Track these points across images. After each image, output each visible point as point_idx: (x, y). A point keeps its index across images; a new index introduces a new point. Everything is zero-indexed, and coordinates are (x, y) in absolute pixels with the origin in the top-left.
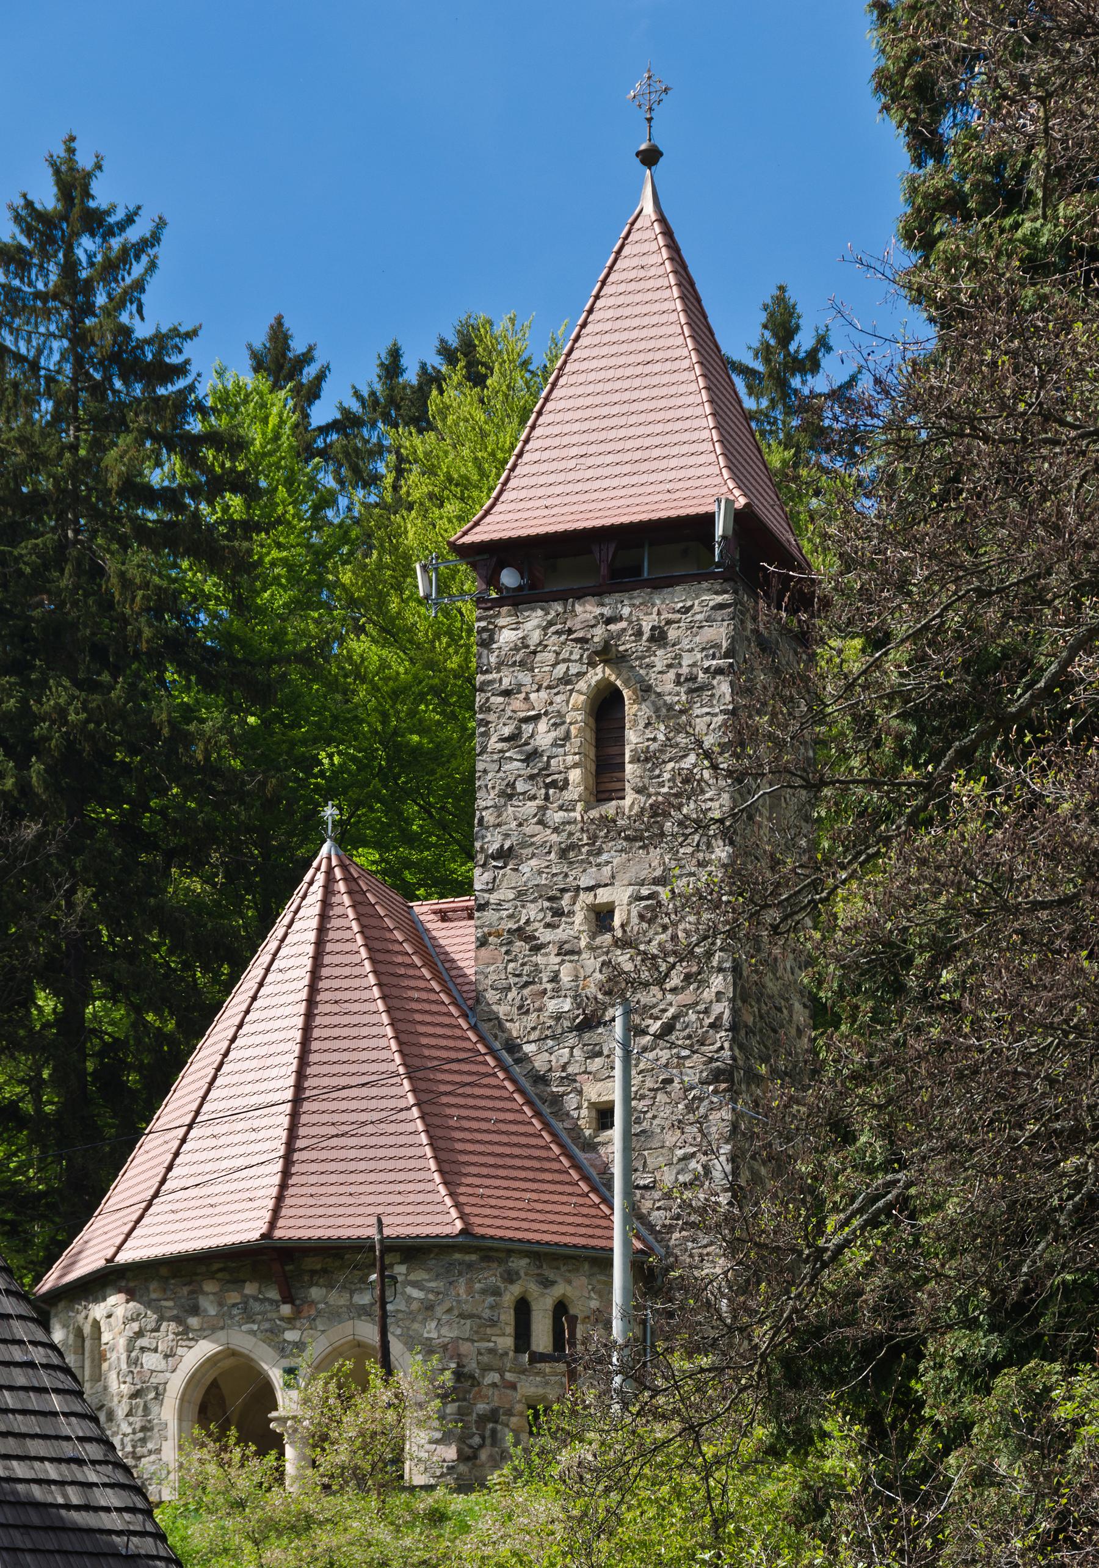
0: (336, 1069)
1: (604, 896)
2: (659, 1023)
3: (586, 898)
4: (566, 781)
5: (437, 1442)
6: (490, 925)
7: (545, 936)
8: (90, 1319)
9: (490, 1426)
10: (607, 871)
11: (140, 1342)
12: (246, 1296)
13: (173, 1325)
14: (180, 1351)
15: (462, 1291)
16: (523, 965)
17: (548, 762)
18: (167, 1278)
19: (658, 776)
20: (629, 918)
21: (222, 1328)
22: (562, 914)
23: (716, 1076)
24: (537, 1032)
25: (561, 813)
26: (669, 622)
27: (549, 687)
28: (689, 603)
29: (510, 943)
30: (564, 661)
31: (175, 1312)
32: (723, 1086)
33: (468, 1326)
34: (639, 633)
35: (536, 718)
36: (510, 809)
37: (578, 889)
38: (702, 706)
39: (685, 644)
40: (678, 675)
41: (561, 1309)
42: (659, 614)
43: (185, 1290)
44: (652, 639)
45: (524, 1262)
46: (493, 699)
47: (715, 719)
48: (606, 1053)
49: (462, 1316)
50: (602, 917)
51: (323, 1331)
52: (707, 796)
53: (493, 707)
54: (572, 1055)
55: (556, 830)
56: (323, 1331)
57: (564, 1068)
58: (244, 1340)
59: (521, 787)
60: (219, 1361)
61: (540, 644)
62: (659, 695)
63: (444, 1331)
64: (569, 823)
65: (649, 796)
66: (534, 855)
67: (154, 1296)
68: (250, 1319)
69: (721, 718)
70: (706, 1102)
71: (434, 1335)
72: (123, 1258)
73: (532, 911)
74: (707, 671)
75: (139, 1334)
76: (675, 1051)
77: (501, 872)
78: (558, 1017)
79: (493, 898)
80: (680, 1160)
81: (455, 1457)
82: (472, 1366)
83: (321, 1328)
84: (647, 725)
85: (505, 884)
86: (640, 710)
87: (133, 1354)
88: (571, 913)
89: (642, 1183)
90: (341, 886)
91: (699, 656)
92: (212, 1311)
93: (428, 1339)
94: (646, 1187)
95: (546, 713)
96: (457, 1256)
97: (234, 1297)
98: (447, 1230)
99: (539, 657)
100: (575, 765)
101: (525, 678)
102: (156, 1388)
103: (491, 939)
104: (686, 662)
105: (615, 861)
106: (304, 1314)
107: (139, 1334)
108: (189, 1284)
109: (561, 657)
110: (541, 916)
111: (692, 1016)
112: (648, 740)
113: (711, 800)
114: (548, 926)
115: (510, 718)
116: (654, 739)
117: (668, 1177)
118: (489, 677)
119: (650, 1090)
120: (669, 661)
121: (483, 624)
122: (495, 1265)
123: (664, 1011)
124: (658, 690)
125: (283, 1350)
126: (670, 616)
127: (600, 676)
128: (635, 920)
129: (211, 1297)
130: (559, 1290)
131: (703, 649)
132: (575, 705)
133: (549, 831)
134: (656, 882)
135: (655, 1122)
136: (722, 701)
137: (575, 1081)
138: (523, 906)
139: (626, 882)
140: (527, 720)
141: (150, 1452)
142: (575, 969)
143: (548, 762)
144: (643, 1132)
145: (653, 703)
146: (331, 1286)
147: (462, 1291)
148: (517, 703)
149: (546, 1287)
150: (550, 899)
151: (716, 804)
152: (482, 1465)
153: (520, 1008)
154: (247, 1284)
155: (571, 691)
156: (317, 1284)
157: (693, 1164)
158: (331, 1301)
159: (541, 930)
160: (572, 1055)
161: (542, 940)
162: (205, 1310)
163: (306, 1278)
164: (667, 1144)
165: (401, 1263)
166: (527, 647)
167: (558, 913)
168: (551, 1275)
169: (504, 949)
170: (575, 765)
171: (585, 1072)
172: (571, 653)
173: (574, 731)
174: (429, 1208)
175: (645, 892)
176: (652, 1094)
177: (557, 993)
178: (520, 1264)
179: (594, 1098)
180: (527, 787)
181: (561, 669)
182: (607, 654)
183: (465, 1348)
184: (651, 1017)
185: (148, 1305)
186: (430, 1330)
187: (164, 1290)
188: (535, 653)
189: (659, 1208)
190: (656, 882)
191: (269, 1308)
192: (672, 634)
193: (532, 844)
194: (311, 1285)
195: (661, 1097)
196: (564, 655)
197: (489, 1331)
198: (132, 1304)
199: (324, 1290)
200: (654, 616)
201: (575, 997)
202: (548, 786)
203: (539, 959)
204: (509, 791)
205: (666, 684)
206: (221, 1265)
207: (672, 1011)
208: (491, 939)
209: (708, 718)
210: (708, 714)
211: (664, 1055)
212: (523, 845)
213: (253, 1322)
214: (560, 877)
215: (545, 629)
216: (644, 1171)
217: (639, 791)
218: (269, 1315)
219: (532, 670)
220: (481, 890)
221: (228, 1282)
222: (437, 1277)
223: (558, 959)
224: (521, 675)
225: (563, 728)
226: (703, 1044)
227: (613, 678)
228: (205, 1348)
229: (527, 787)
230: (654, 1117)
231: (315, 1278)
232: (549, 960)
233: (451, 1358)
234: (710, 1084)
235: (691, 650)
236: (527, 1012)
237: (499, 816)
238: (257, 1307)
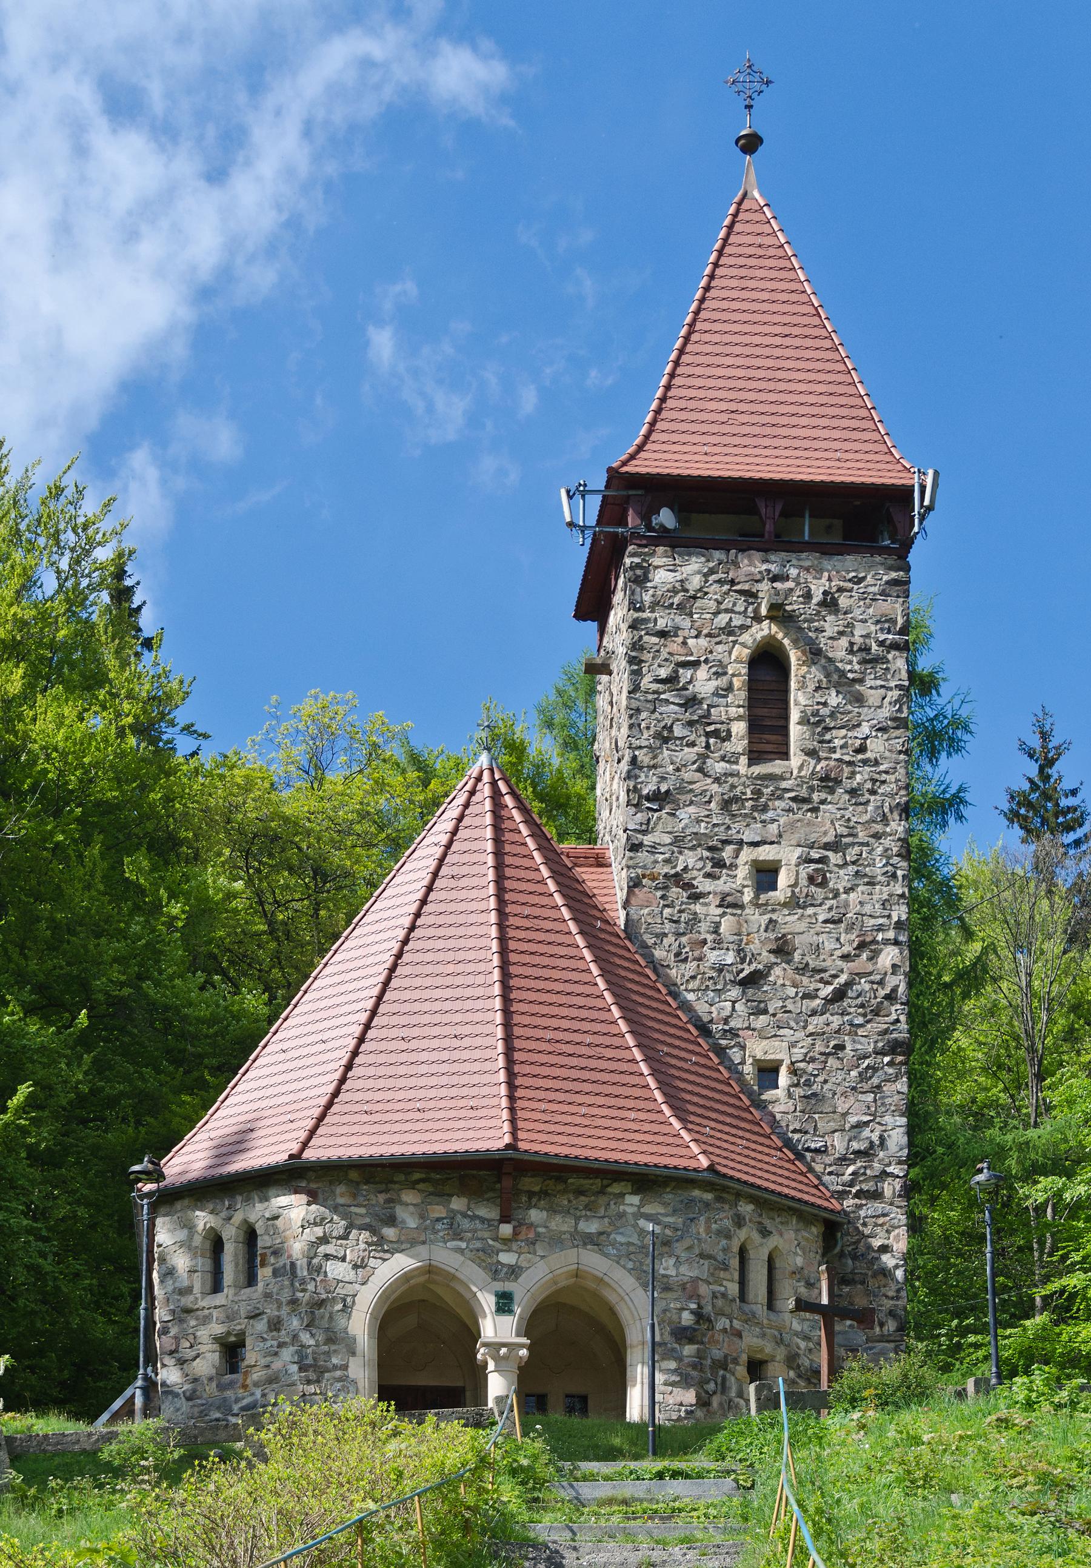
0: (541, 984)
1: (766, 853)
2: (830, 988)
3: (747, 855)
4: (729, 732)
5: (673, 1384)
6: (644, 867)
7: (704, 885)
9: (721, 1372)
10: (773, 828)
11: (323, 1249)
12: (453, 1211)
13: (365, 1235)
14: (372, 1262)
15: (701, 1230)
16: (680, 911)
17: (708, 710)
18: (358, 1183)
19: (829, 742)
20: (797, 879)
21: (424, 1243)
22: (724, 866)
23: (894, 1048)
24: (697, 982)
25: (723, 764)
26: (840, 590)
27: (709, 635)
28: (862, 575)
29: (666, 888)
30: (727, 611)
31: (367, 1220)
32: (900, 1058)
33: (706, 1267)
34: (808, 596)
35: (696, 664)
36: (666, 753)
37: (741, 843)
38: (875, 678)
39: (857, 613)
40: (852, 644)
42: (830, 580)
43: (381, 1198)
44: (823, 604)
45: (750, 1207)
46: (646, 638)
47: (890, 694)
48: (771, 1011)
49: (702, 1256)
50: (765, 875)
51: (543, 1257)
52: (882, 768)
53: (647, 646)
54: (733, 1009)
55: (717, 780)
56: (543, 1257)
57: (726, 1021)
58: (448, 1256)
59: (678, 731)
60: (412, 1278)
61: (700, 590)
62: (830, 660)
63: (683, 1269)
64: (732, 775)
65: (819, 760)
66: (692, 803)
68: (458, 1236)
69: (896, 693)
70: (880, 1073)
71: (672, 1272)
72: (309, 1155)
73: (689, 859)
74: (881, 644)
75: (324, 1240)
76: (846, 1018)
77: (656, 815)
78: (720, 969)
79: (647, 840)
80: (853, 1127)
81: (694, 1401)
82: (708, 1309)
83: (540, 1253)
84: (818, 689)
85: (660, 827)
86: (809, 672)
87: (315, 1261)
88: (733, 866)
89: (813, 1146)
90: (508, 800)
91: (873, 628)
92: (412, 1223)
93: (664, 1276)
94: (817, 1151)
95: (706, 661)
96: (696, 1193)
97: (438, 1211)
98: (693, 1164)
99: (699, 603)
100: (739, 718)
101: (685, 623)
102: (344, 1300)
103: (644, 881)
104: (858, 632)
105: (782, 820)
106: (522, 1237)
107: (324, 1240)
108: (387, 1191)
109: (723, 607)
110: (700, 864)
111: (864, 985)
112: (818, 703)
113: (887, 772)
114: (708, 875)
115: (666, 660)
116: (825, 704)
117: (839, 1143)
118: (645, 615)
119: (821, 1054)
120: (841, 629)
121: (637, 560)
122: (727, 1207)
123: (835, 976)
124: (830, 655)
125: (495, 1272)
126: (842, 584)
127: (766, 632)
128: (803, 882)
129: (411, 1208)
130: (774, 1241)
131: (878, 622)
132: (737, 657)
133: (709, 781)
134: (826, 846)
135: (826, 1087)
136: (897, 676)
137: (738, 1036)
138: (680, 853)
139: (794, 842)
140: (685, 665)
141: (336, 1367)
142: (738, 922)
143: (708, 710)
144: (814, 1095)
145: (824, 668)
146: (553, 1210)
147: (701, 1230)
148: (674, 646)
149: (764, 1236)
150: (710, 849)
151: (892, 778)
152: (715, 1413)
153: (677, 955)
154: (454, 1199)
155: (735, 642)
156: (535, 1206)
157: (866, 1133)
158: (553, 1225)
159: (700, 879)
160: (733, 1009)
161: (700, 889)
162: (403, 1222)
163: (524, 1199)
164: (839, 1110)
165: (633, 1193)
166: (687, 591)
167: (719, 864)
168: (767, 1223)
169: (659, 894)
170: (739, 718)
171: (748, 1028)
172: (734, 604)
173: (737, 683)
174: (660, 1139)
175: (815, 854)
176: (823, 1058)
177: (718, 944)
178: (746, 1209)
179: (759, 1055)
180: (685, 732)
181: (722, 619)
182: (779, 614)
183: (704, 1289)
184: (821, 980)
185: (335, 1209)
186: (667, 1267)
187: (354, 1196)
188: (694, 598)
189: (830, 1173)
190: (826, 846)
191: (479, 1226)
192: (843, 601)
193: (691, 791)
194: (529, 1208)
195: (832, 1062)
196: (727, 604)
197: (722, 1274)
198: (314, 1207)
199: (545, 1213)
200: (824, 581)
201: (739, 951)
202: (708, 735)
203: (698, 908)
204: (665, 734)
205: (839, 650)
206: (423, 1176)
207: (843, 978)
208: (644, 881)
209: (883, 691)
210: (882, 687)
211: (836, 1021)
212: (681, 790)
213: (461, 1239)
214: (722, 828)
215: (706, 575)
216: (814, 1135)
217: (812, 753)
218: (480, 1234)
219: (691, 615)
220: (635, 830)
221: (431, 1194)
222: (675, 1212)
223: (720, 911)
224: (678, 619)
225: (725, 679)
226: (877, 1015)
227: (780, 636)
228: (400, 1263)
229: (685, 732)
230: (826, 1081)
231: (534, 1200)
232: (708, 910)
233: (690, 1297)
234: (885, 1055)
235: (865, 621)
236: (685, 960)
237: (655, 757)
238: (466, 1224)
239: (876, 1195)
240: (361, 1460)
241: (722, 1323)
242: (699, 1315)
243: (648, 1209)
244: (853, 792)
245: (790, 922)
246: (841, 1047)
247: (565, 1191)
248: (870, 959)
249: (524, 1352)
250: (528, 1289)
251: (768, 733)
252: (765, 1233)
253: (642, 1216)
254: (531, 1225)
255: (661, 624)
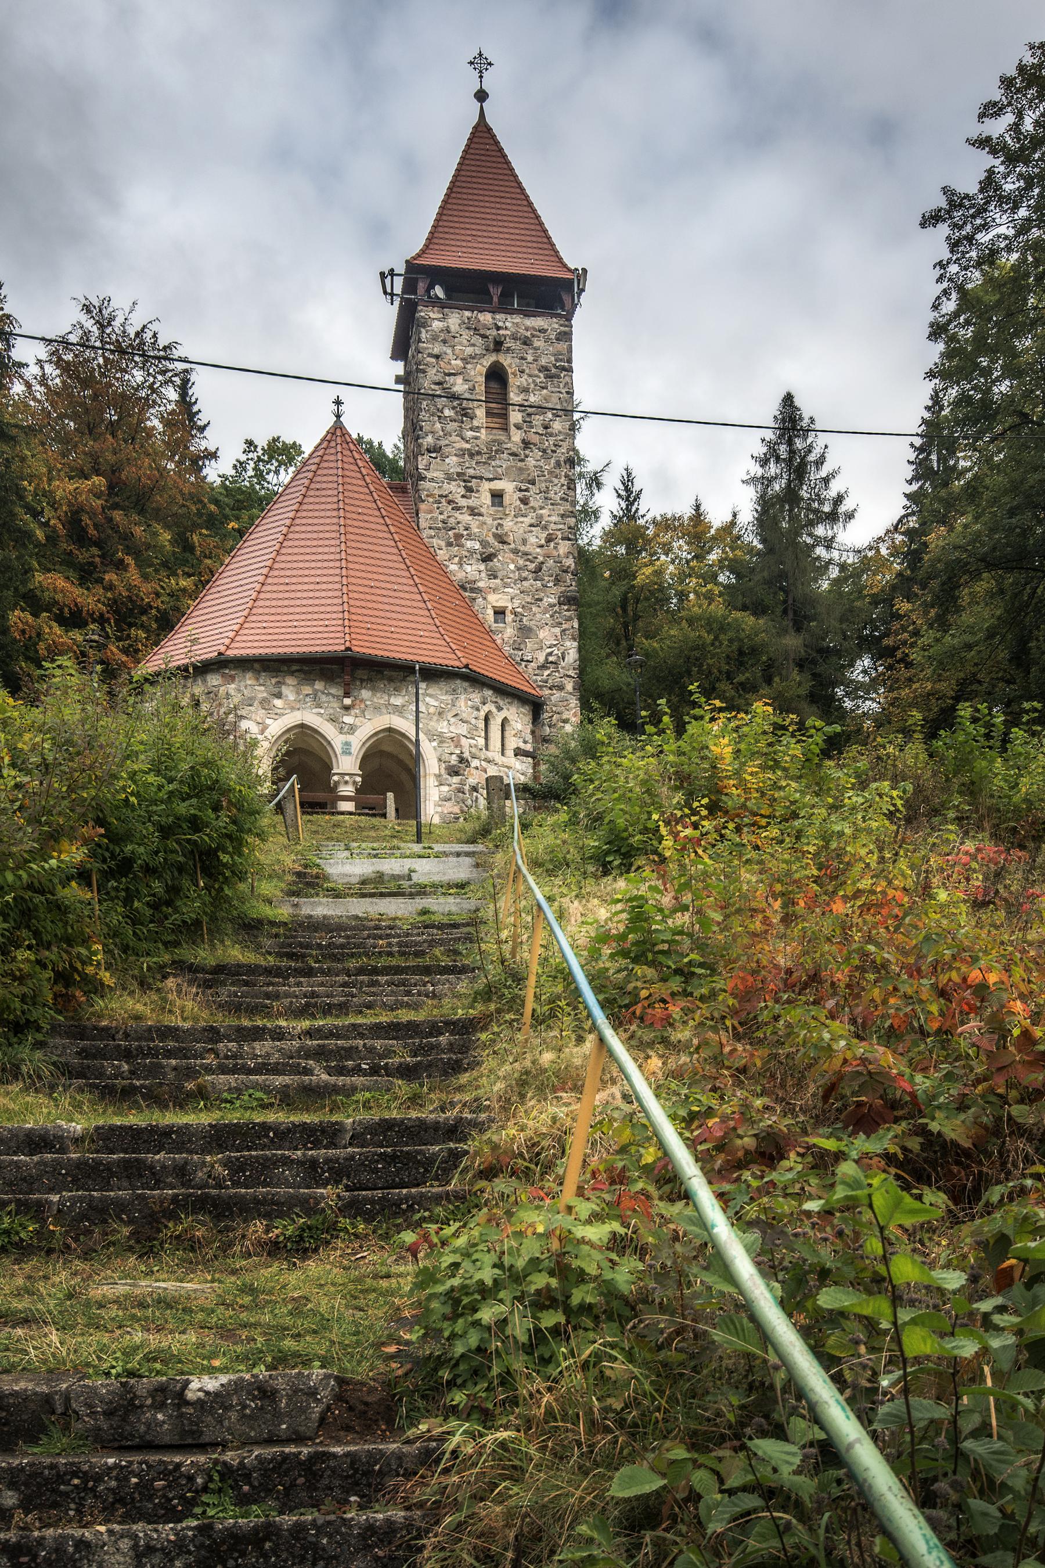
1: (497, 485)
8: (569, 697)
37: (481, 478)
41: (504, 723)
43: (274, 681)
45: (490, 692)
67: (249, 682)
72: (231, 653)
74: (557, 368)
82: (466, 755)
92: (292, 697)
97: (307, 690)
114: (463, 496)
130: (504, 714)
132: (478, 372)
146: (374, 689)
167: (470, 490)
168: (501, 703)
178: (488, 693)
181: (469, 350)
187: (257, 679)
192: (537, 343)
238: (324, 698)
239: (561, 688)
240: (522, 372)
241: (475, 763)
242: (462, 760)
243: (430, 691)
244: (544, 451)
245: (508, 524)
246: (541, 600)
247: (382, 679)
248: (555, 548)
249: (359, 779)
250: (358, 741)
251: (499, 413)
252: (500, 709)
253: (433, 697)
254: (362, 701)
255: (436, 351)
